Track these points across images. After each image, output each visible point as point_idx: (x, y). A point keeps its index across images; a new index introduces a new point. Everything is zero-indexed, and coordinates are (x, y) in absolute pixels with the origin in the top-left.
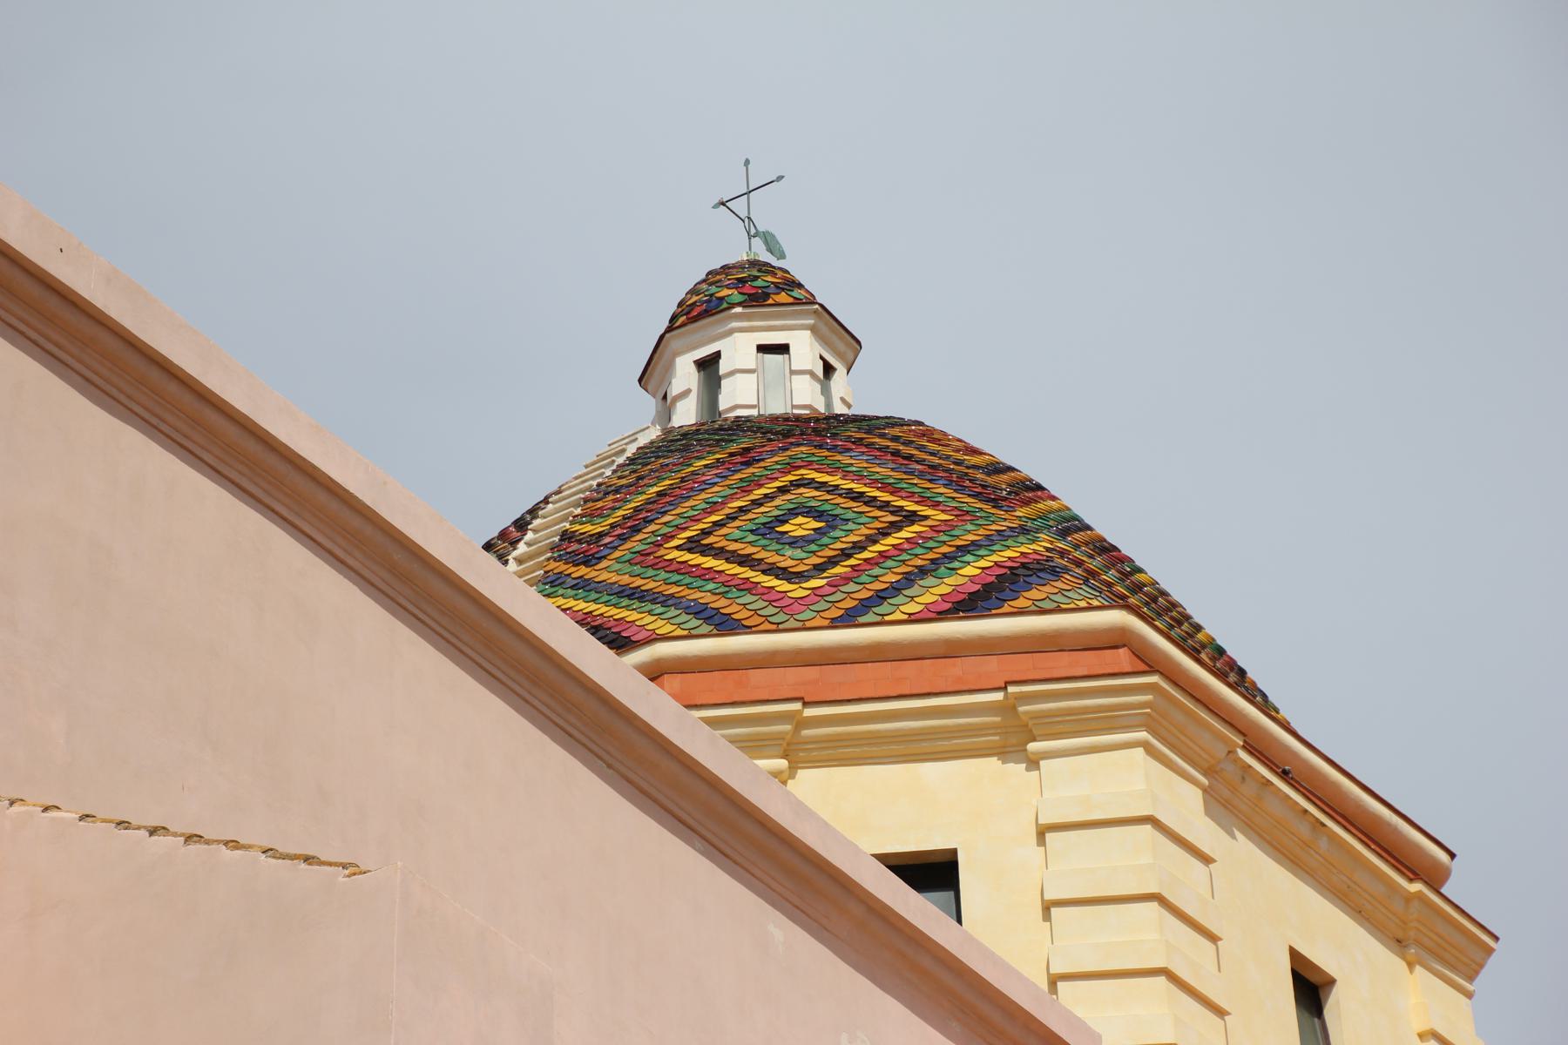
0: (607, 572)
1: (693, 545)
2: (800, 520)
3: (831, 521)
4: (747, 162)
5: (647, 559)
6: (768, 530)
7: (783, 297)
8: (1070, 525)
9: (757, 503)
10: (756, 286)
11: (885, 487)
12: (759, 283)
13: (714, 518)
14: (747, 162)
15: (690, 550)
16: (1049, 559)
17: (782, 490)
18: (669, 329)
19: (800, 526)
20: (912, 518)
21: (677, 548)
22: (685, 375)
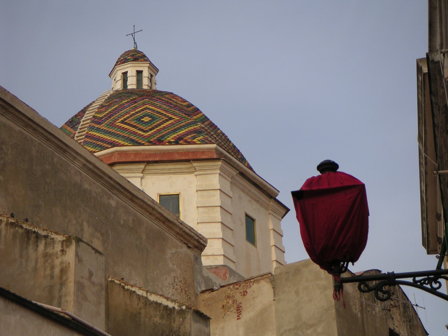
0: (103, 127)
1: (123, 122)
2: (146, 117)
3: (153, 119)
4: (134, 26)
5: (112, 125)
6: (139, 120)
7: (142, 59)
8: (205, 119)
9: (137, 113)
10: (136, 56)
11: (165, 111)
12: (137, 56)
13: (127, 116)
14: (134, 26)
15: (122, 123)
16: (200, 129)
17: (142, 110)
18: (116, 65)
19: (146, 119)
20: (170, 119)
21: (119, 122)
22: (119, 75)
